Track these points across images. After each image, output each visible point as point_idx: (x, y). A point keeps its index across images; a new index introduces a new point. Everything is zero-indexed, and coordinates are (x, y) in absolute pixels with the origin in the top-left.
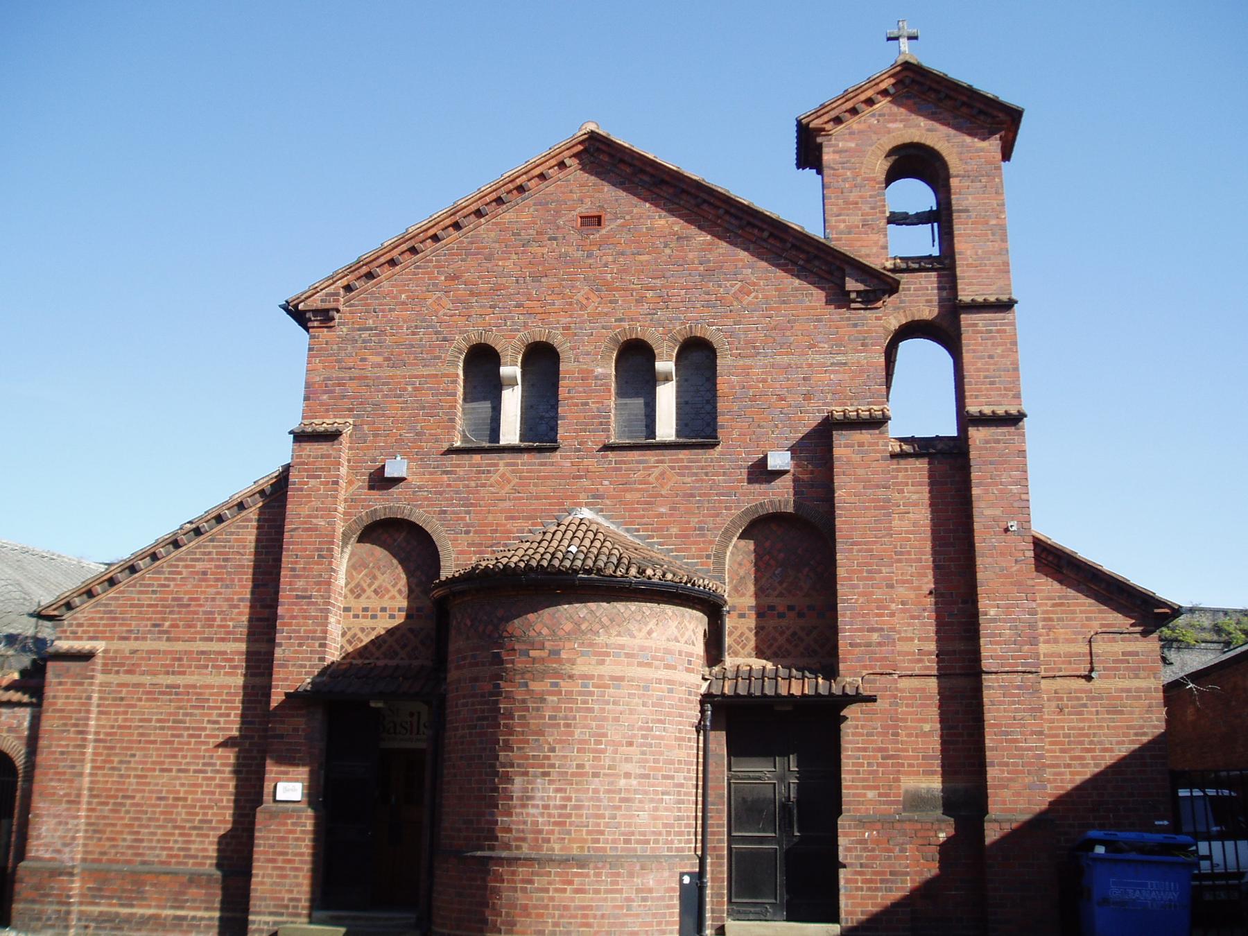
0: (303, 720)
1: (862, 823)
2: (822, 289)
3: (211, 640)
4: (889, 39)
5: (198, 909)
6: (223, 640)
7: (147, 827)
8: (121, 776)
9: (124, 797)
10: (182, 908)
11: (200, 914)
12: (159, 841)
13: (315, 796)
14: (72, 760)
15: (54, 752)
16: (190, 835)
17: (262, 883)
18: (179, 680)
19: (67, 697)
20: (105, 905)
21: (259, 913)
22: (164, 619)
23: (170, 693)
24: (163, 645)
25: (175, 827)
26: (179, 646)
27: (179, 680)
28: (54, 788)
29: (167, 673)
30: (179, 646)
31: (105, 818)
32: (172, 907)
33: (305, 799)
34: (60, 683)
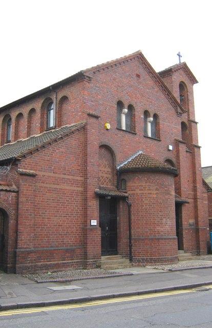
0: (95, 201)
1: (186, 229)
2: (192, 89)
3: (65, 174)
4: (97, 117)
5: (69, 260)
6: (68, 175)
7: (52, 235)
8: (43, 218)
9: (44, 225)
10: (65, 260)
11: (60, 262)
12: (55, 239)
13: (101, 224)
14: (31, 212)
15: (24, 210)
16: (64, 237)
17: (90, 250)
18: (58, 187)
19: (27, 190)
20: (43, 262)
21: (89, 259)
22: (52, 166)
23: (55, 191)
24: (51, 174)
25: (60, 235)
26: (57, 175)
27: (58, 187)
28: (25, 222)
29: (54, 184)
30: (57, 175)
31: (39, 232)
32: (71, 260)
33: (99, 225)
34: (25, 185)
